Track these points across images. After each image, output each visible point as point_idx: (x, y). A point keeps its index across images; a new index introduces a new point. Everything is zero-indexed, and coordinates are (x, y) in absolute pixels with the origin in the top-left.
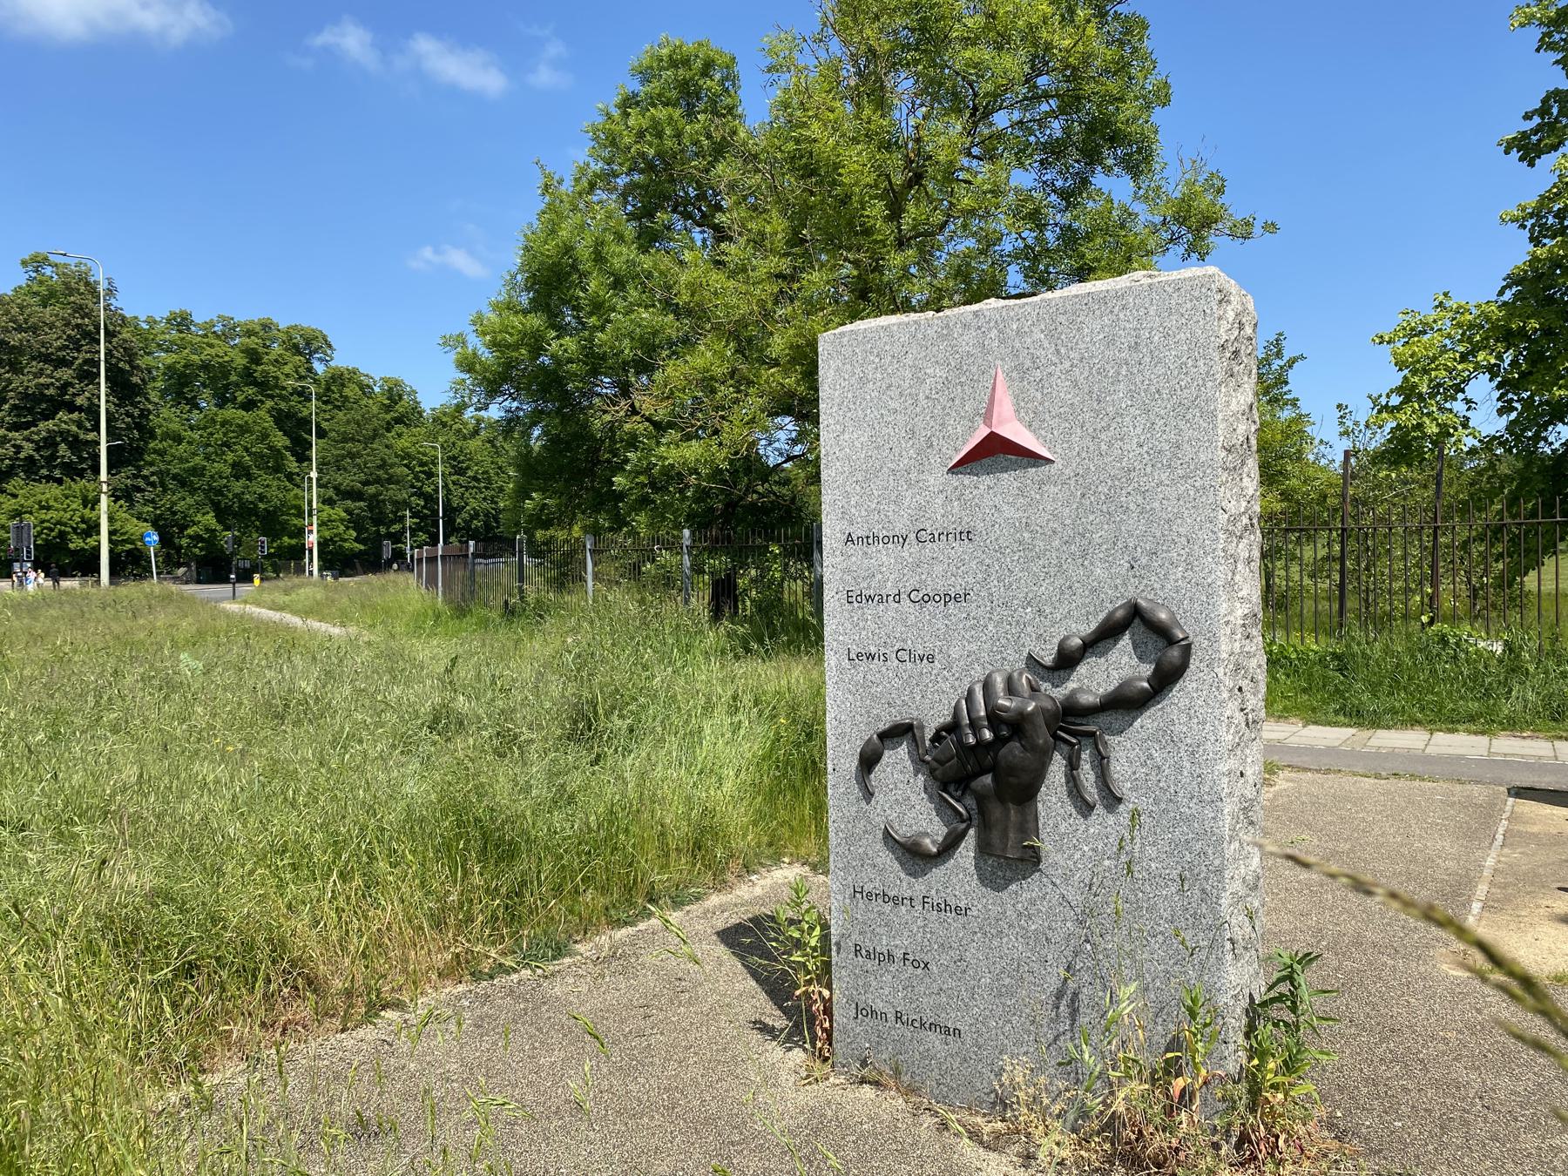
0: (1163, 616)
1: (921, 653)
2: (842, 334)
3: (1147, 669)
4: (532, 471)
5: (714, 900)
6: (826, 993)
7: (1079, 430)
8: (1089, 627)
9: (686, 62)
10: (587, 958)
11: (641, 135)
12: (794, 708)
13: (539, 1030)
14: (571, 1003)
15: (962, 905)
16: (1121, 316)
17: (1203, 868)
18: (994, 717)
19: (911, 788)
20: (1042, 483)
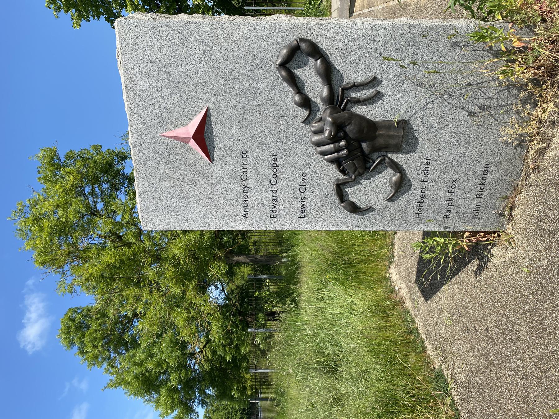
0: (285, 51)
1: (301, 180)
2: (143, 217)
3: (311, 61)
4: (223, 394)
5: (409, 304)
6: (467, 234)
7: (193, 94)
8: (290, 90)
9: (68, 328)
10: (443, 362)
11: (95, 346)
12: (321, 271)
13: (488, 384)
14: (470, 368)
15: (425, 161)
16: (137, 70)
17: (409, 35)
18: (334, 139)
19: (368, 186)
20: (219, 113)
